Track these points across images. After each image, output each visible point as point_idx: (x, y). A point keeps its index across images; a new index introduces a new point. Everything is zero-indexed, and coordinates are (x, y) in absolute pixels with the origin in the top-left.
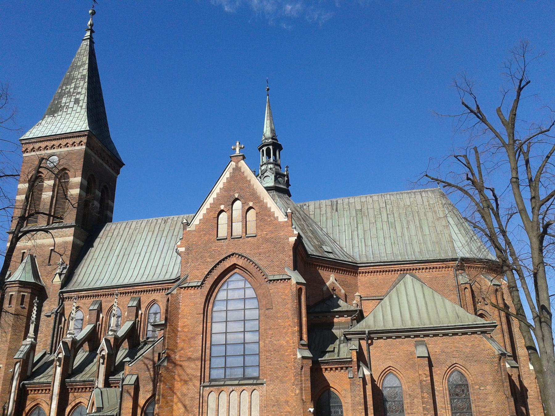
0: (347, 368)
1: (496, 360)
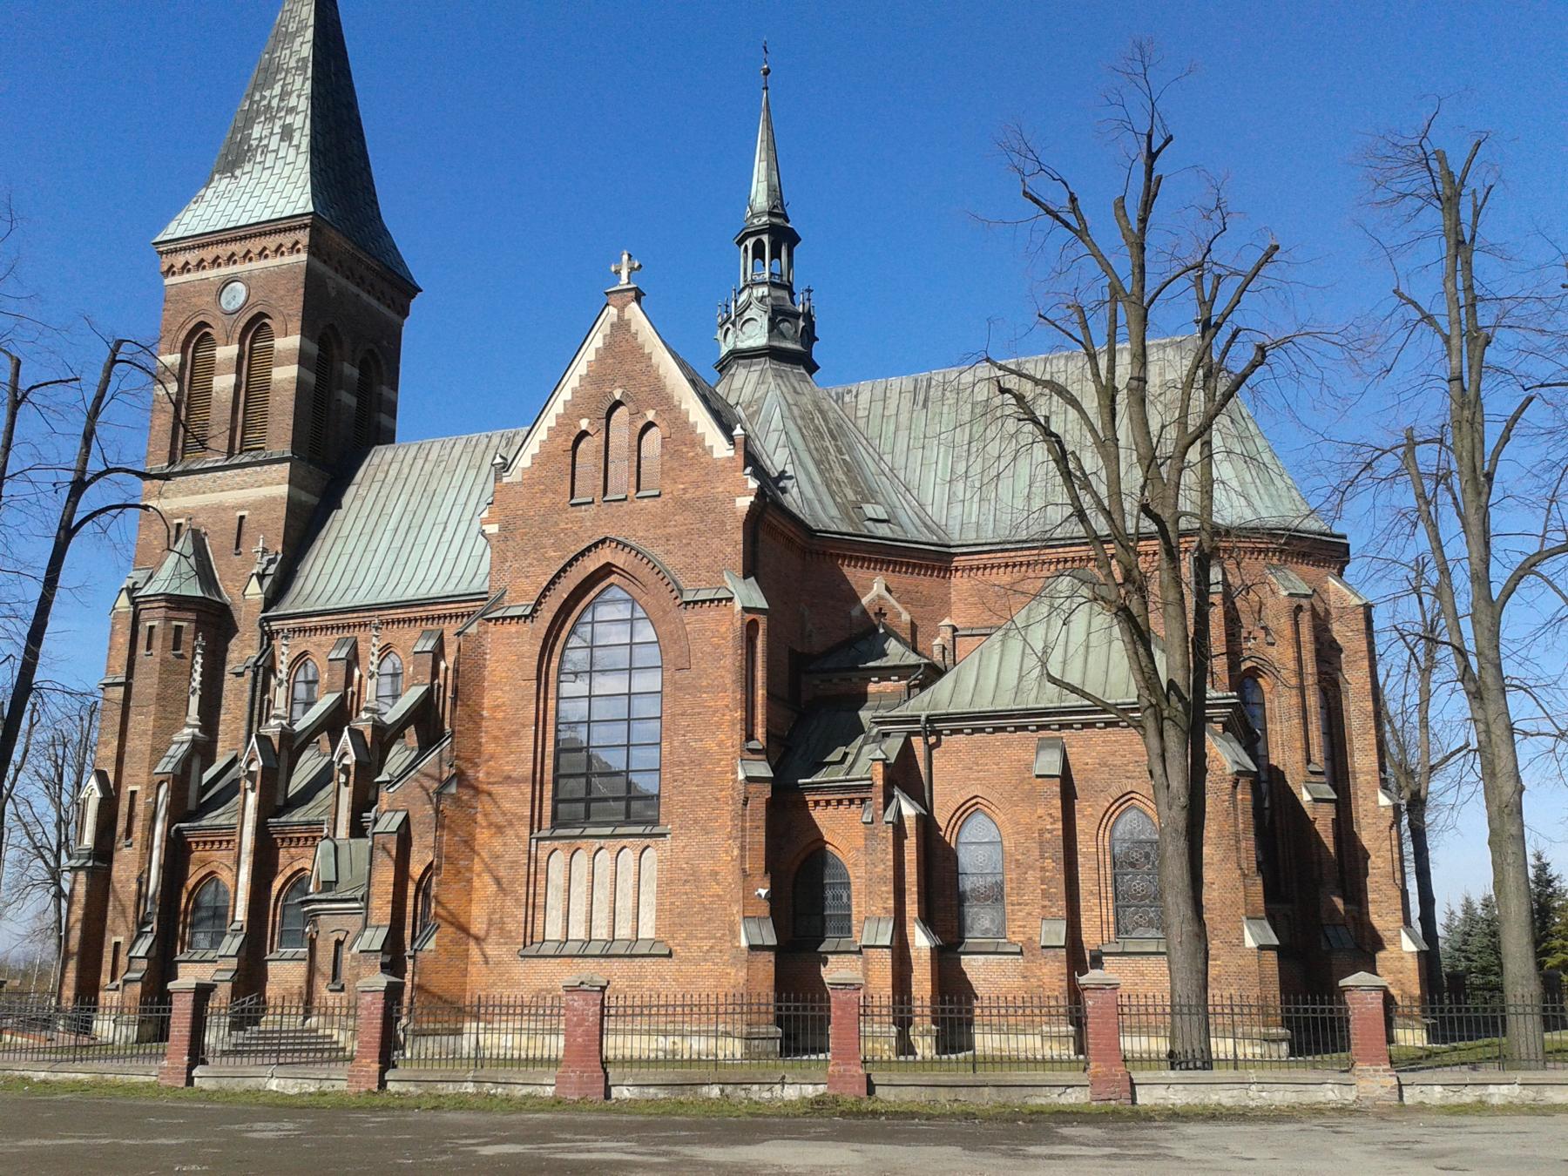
0: (863, 801)
1: (1227, 785)
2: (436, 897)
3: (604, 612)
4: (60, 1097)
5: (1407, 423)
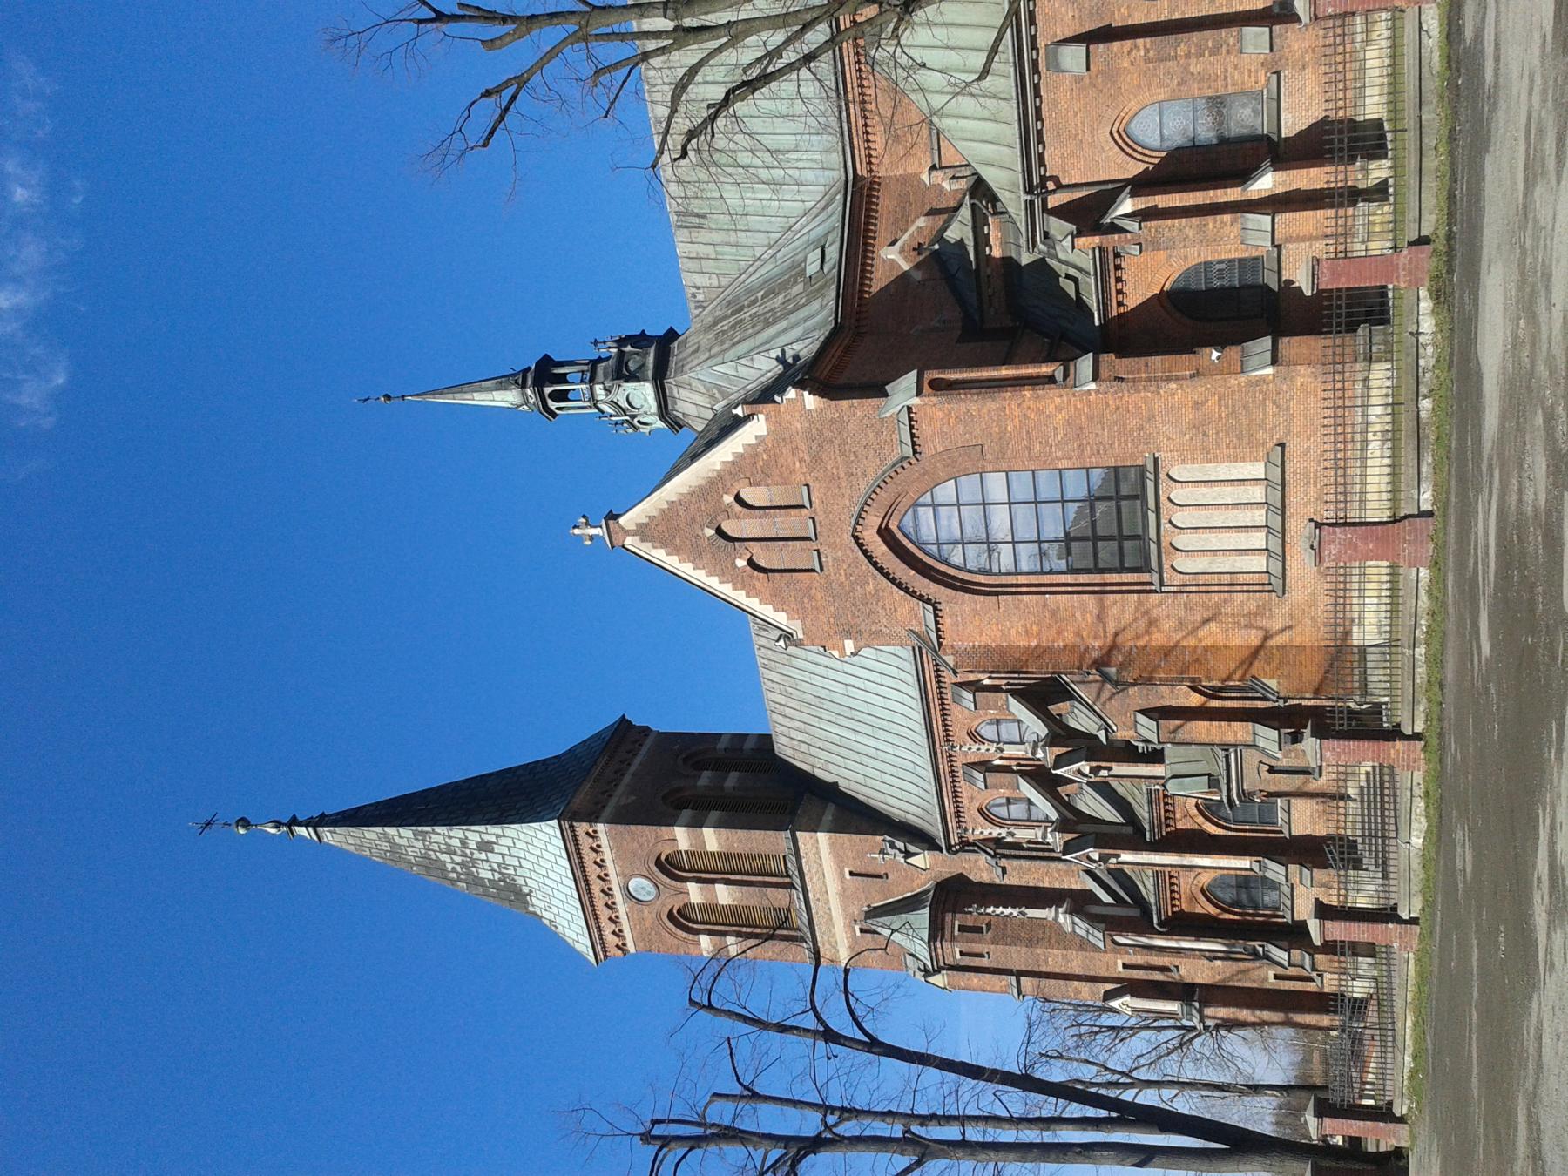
0: (1117, 255)
2: (1224, 681)
3: (927, 532)
4: (1436, 969)
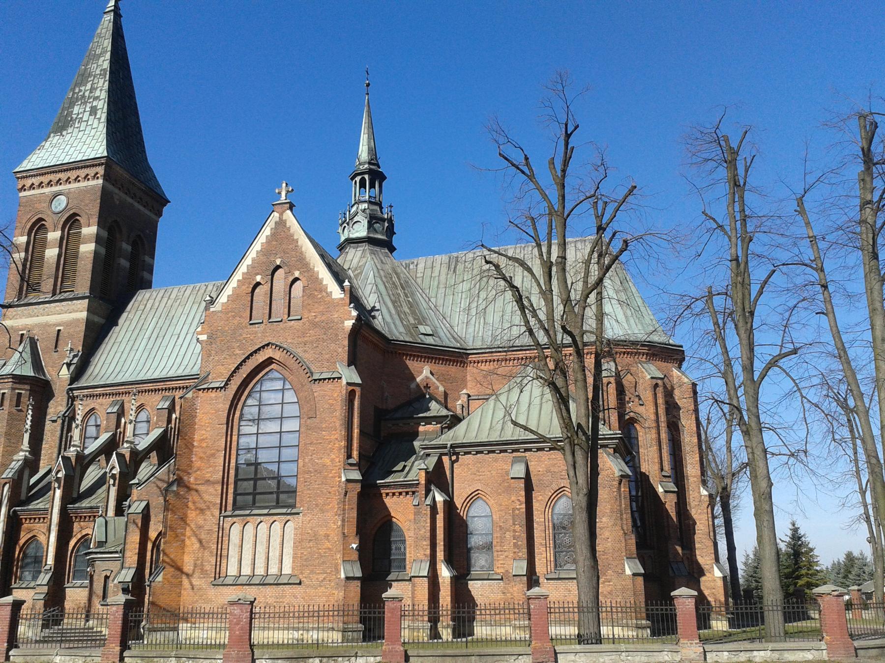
0: (414, 493)
1: (616, 483)
2: (163, 550)
3: (267, 385)
5: (709, 284)
